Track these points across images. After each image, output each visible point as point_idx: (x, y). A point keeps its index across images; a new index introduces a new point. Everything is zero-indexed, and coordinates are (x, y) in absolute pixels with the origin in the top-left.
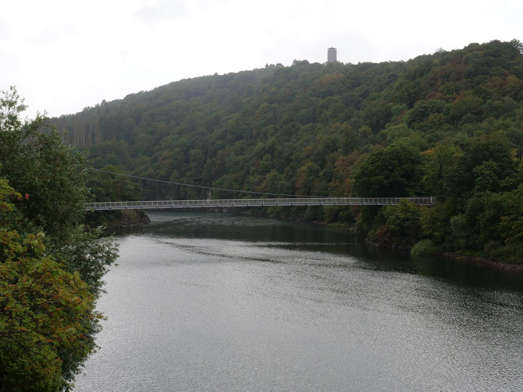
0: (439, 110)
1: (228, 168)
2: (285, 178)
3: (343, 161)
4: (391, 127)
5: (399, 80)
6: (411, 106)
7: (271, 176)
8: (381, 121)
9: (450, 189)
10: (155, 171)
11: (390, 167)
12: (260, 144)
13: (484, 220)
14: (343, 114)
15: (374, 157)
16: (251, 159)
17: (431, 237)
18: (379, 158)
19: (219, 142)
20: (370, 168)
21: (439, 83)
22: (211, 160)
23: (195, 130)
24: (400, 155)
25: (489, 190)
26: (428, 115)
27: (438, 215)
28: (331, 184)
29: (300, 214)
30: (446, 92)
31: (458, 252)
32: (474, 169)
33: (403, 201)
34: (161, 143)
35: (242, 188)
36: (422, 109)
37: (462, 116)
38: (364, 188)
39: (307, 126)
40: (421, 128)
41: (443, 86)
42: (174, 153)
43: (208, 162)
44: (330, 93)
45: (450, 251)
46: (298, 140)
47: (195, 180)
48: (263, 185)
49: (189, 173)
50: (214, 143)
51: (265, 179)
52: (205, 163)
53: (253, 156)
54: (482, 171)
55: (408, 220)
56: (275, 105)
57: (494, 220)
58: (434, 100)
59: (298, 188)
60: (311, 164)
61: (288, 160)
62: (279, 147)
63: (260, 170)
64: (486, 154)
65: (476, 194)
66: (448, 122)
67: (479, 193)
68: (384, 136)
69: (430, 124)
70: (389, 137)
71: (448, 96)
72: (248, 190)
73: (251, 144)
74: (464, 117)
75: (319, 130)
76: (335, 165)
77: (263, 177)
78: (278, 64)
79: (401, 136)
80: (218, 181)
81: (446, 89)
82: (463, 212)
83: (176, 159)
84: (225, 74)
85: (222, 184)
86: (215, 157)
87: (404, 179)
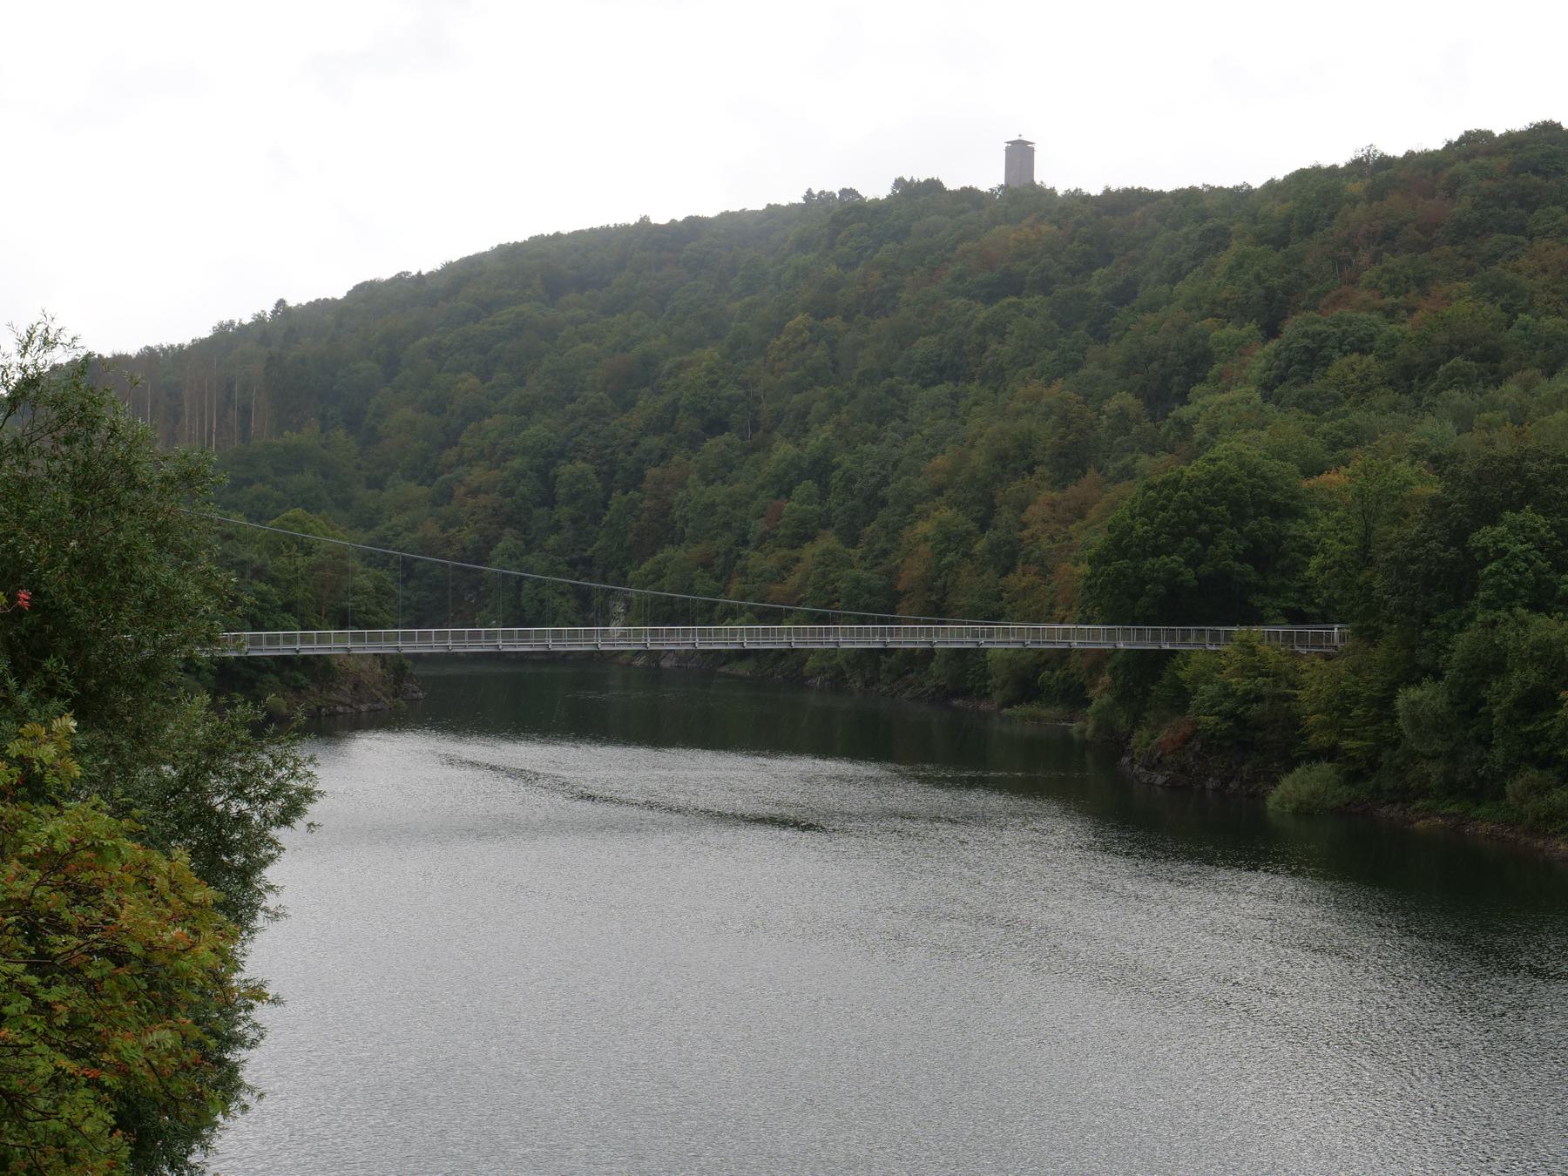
0: (1362, 346)
1: (679, 525)
2: (863, 558)
3: (1053, 505)
4: (1207, 399)
5: (1236, 246)
6: (1271, 331)
7: (817, 552)
8: (1176, 379)
9: (1396, 600)
10: (443, 530)
11: (1204, 528)
12: (783, 450)
13: (1506, 702)
14: (1054, 354)
15: (1151, 493)
16: (754, 497)
17: (1331, 753)
18: (1169, 499)
19: (653, 441)
20: (1140, 530)
21: (1364, 257)
22: (625, 499)
23: (573, 400)
24: (1237, 490)
25: (1525, 606)
26: (1328, 361)
27: (1357, 684)
28: (1012, 579)
29: (911, 676)
30: (1386, 287)
31: (1419, 804)
32: (1476, 536)
33: (1245, 636)
34: (463, 439)
35: (725, 591)
36: (1307, 342)
37: (1436, 365)
38: (1117, 598)
39: (936, 390)
40: (1304, 402)
41: (1377, 268)
42: (506, 474)
43: (614, 504)
44: (1012, 285)
45: (1394, 802)
46: (908, 434)
47: (573, 564)
48: (793, 580)
49: (552, 540)
50: (635, 444)
51: (798, 560)
52: (606, 506)
53: (762, 487)
54: (1501, 545)
55: (1259, 699)
56: (836, 322)
57: (1537, 702)
58: (1348, 313)
59: (905, 592)
60: (947, 514)
61: (875, 502)
62: (845, 459)
63: (782, 531)
64: (1515, 488)
65: (1480, 617)
66: (1390, 382)
67: (1491, 615)
68: (1185, 427)
69: (1333, 391)
70: (1200, 432)
71: (1390, 300)
72: (743, 598)
73: (755, 449)
74: (1442, 368)
75: (976, 404)
76: (1025, 517)
77: (795, 553)
78: (844, 192)
79: (1240, 427)
80: (647, 566)
81: (1387, 277)
82: (1438, 676)
83: (510, 493)
84: (673, 221)
85: (659, 575)
86: (639, 490)
87: (1249, 567)
